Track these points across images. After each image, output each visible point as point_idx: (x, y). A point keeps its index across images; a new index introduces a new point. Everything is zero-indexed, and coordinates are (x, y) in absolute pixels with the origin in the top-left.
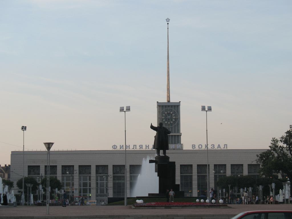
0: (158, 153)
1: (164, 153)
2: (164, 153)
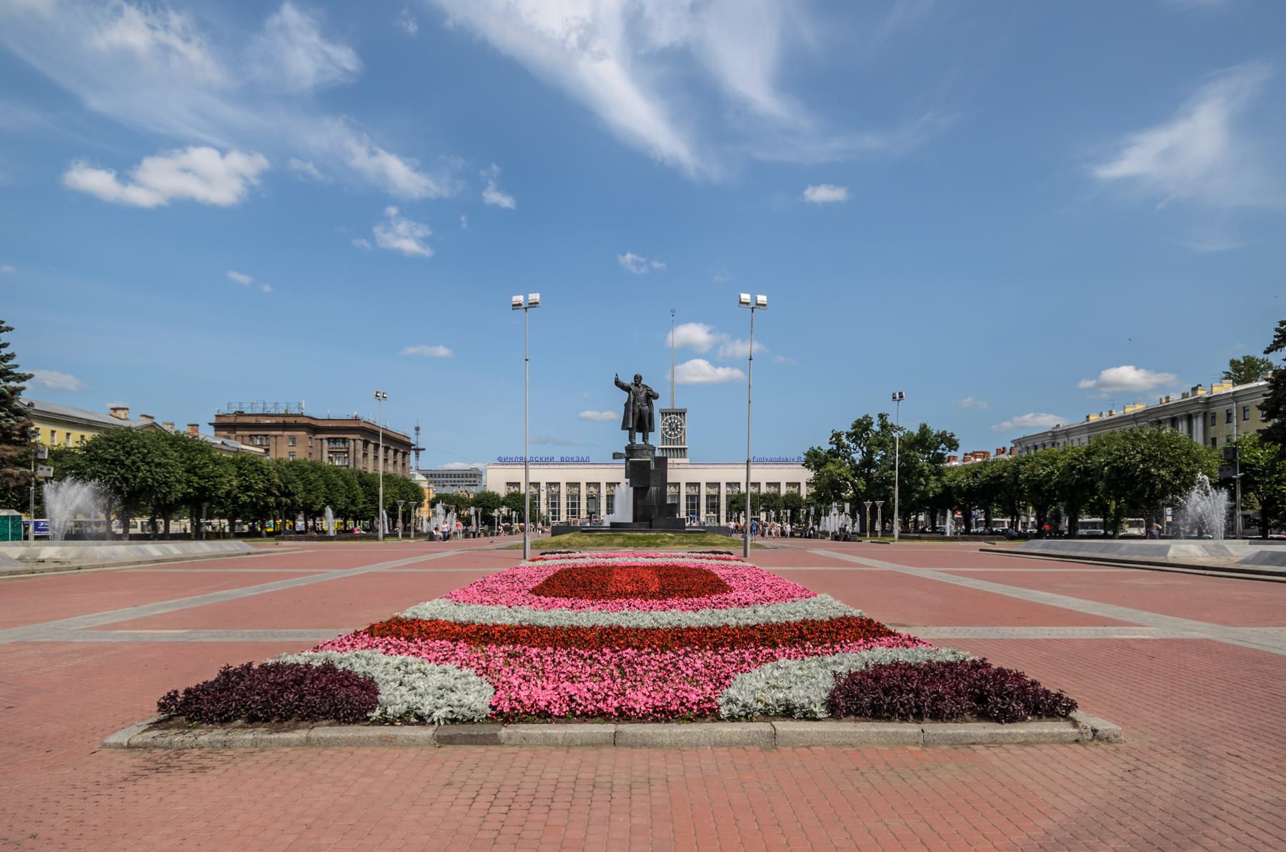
0: (631, 437)
1: (645, 438)
2: (645, 438)
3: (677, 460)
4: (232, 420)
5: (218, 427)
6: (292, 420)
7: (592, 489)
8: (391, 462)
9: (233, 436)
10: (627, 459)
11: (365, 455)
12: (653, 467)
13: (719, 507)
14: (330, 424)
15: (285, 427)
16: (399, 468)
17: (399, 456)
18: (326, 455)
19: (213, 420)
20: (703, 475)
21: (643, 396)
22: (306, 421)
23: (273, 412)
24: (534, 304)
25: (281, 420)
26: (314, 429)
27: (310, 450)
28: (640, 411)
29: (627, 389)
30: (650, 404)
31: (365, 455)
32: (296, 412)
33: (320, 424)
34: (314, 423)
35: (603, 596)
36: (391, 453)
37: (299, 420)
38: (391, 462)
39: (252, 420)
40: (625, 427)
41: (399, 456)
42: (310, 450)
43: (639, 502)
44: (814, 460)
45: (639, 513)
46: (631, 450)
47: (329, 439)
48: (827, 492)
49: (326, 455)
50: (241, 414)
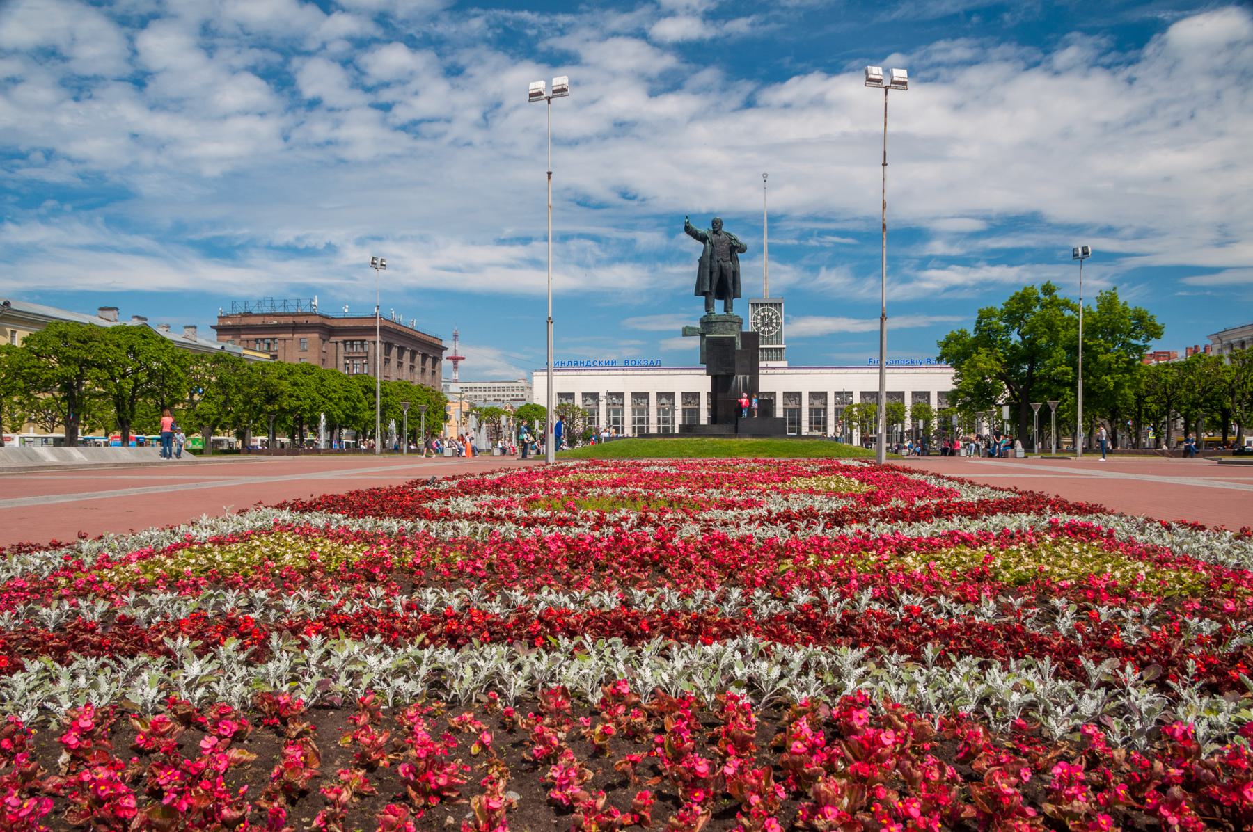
0: (708, 306)
3: (772, 364)
4: (236, 322)
5: (221, 330)
6: (302, 320)
7: (664, 400)
8: (418, 369)
9: (238, 340)
10: (702, 335)
11: (387, 361)
12: (739, 346)
13: (825, 422)
14: (347, 324)
15: (295, 328)
16: (428, 377)
17: (429, 362)
18: (341, 361)
19: (216, 323)
20: (806, 382)
21: (725, 246)
22: (317, 320)
23: (280, 310)
24: (561, 91)
25: (290, 320)
26: (328, 330)
27: (323, 356)
28: (721, 268)
29: (702, 238)
30: (735, 260)
31: (387, 361)
32: (307, 310)
33: (335, 324)
34: (328, 322)
35: (412, 513)
36: (419, 358)
37: (312, 320)
38: (418, 369)
39: (259, 321)
40: (699, 291)
41: (429, 362)
42: (323, 356)
43: (720, 397)
44: (956, 353)
45: (721, 413)
46: (707, 323)
47: (345, 342)
48: (973, 398)
49: (341, 361)
50: (249, 314)
